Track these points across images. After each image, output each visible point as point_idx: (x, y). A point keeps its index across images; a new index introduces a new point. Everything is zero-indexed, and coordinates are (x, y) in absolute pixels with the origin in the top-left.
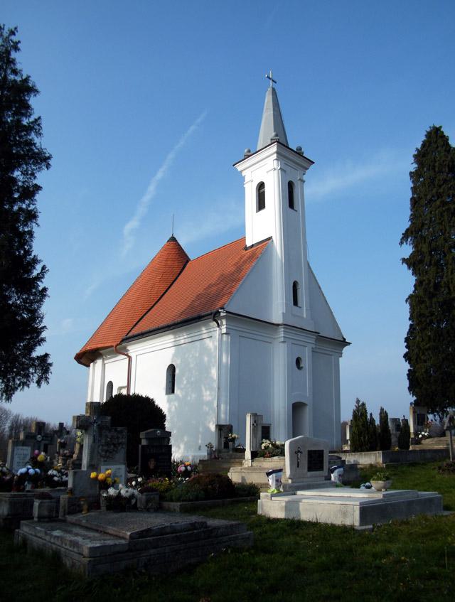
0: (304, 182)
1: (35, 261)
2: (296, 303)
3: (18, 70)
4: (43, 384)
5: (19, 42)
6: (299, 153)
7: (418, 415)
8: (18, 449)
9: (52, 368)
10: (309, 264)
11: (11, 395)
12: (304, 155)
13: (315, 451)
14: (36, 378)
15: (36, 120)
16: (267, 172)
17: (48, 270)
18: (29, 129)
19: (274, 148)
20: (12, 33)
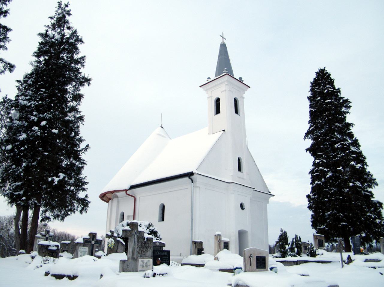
0: (244, 98)
1: (80, 140)
2: (240, 169)
3: (71, 27)
4: (84, 213)
5: (70, 10)
6: (240, 80)
7: (319, 240)
8: (81, 248)
9: (89, 204)
10: (247, 147)
11: (64, 218)
12: (243, 82)
13: (261, 257)
14: (79, 209)
15: (82, 58)
16: (222, 92)
17: (90, 148)
18: (77, 62)
19: (3, 5)
20: (67, 6)
